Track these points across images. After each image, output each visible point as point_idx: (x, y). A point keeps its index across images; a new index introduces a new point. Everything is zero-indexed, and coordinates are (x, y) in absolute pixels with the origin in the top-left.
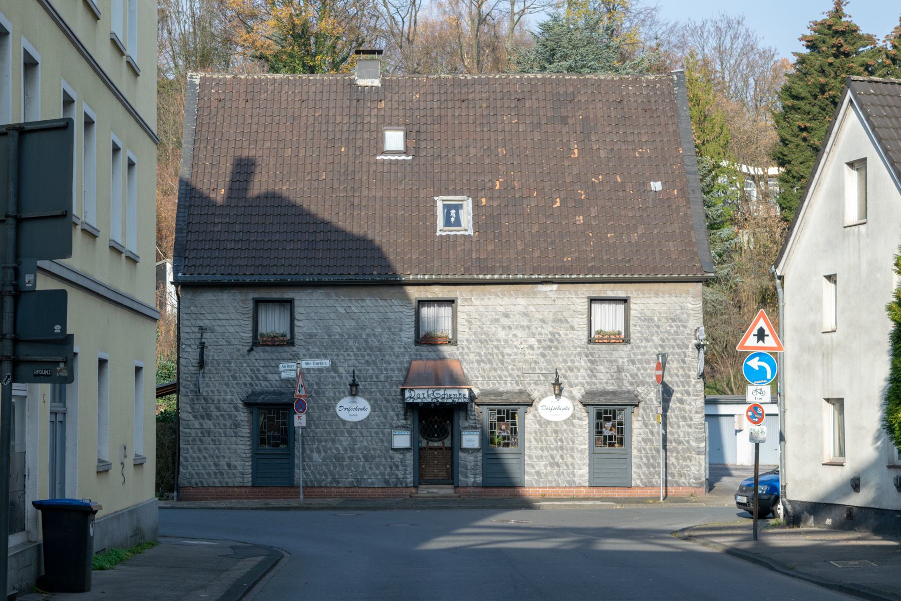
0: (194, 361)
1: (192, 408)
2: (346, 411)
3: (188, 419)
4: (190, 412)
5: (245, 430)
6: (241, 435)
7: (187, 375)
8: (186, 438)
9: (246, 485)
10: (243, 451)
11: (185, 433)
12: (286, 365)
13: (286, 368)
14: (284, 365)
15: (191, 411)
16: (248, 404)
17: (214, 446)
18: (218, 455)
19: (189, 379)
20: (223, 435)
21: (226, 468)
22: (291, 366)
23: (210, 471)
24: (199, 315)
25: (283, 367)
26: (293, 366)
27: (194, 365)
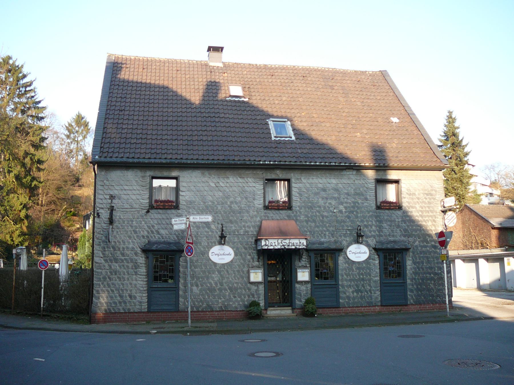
0: (106, 220)
1: (103, 254)
2: (354, 254)
3: (100, 262)
4: (102, 257)
5: (143, 270)
6: (140, 274)
7: (100, 230)
8: (98, 276)
9: (143, 311)
10: (141, 286)
11: (98, 272)
12: (177, 219)
13: (178, 222)
14: (176, 219)
15: (102, 256)
16: (145, 251)
17: (119, 282)
18: (123, 288)
19: (102, 233)
20: (126, 274)
21: (128, 298)
22: (182, 220)
23: (116, 301)
24: (109, 186)
25: (175, 221)
26: (184, 220)
27: (106, 222)
